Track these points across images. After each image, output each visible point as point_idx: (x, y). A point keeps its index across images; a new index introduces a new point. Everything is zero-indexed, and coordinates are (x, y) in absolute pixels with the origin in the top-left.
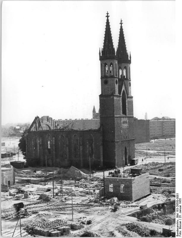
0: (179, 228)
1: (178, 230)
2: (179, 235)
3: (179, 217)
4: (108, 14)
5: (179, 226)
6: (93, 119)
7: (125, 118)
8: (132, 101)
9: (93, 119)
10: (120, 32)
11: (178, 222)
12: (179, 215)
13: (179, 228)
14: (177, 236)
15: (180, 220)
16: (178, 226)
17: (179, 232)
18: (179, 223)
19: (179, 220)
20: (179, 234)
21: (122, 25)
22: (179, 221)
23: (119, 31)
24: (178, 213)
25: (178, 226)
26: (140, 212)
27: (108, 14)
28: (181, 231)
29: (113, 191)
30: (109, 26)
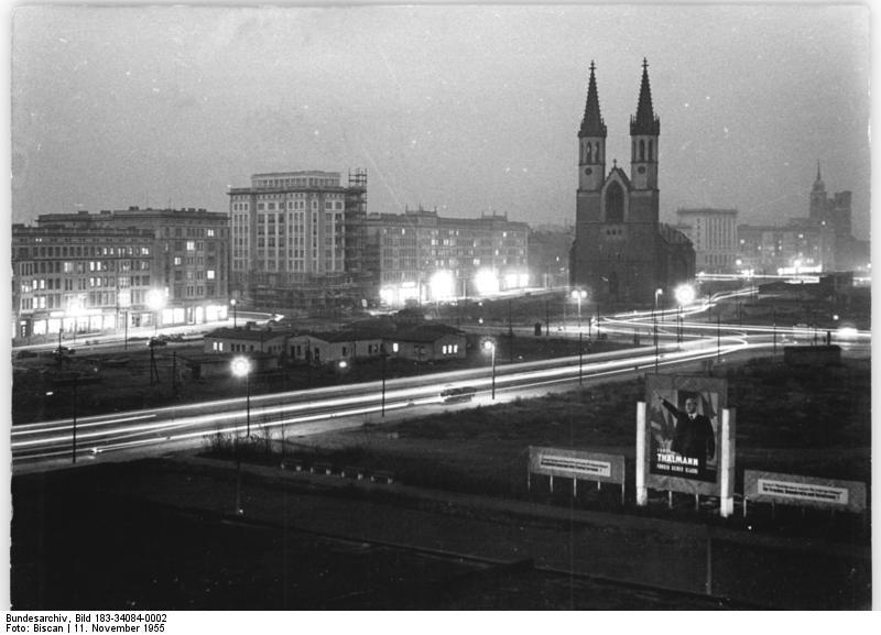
0: (38, 623)
1: (31, 619)
2: (11, 622)
3: (79, 624)
4: (593, 64)
5: (43, 624)
6: (762, 296)
7: (74, 8)
8: (15, 422)
9: (762, 296)
10: (590, 88)
11: (59, 620)
12: (85, 624)
13: (38, 623)
14: (8, 618)
15: (66, 628)
16: (43, 619)
17: (21, 624)
18: (57, 624)
19: (65, 625)
20: (16, 624)
21: (648, 68)
22: (61, 624)
23: (589, 81)
24: (93, 619)
25: (43, 619)
26: (374, 295)
27: (593, 64)
28: (99, 613)
29: (669, 439)
30: (595, 84)
